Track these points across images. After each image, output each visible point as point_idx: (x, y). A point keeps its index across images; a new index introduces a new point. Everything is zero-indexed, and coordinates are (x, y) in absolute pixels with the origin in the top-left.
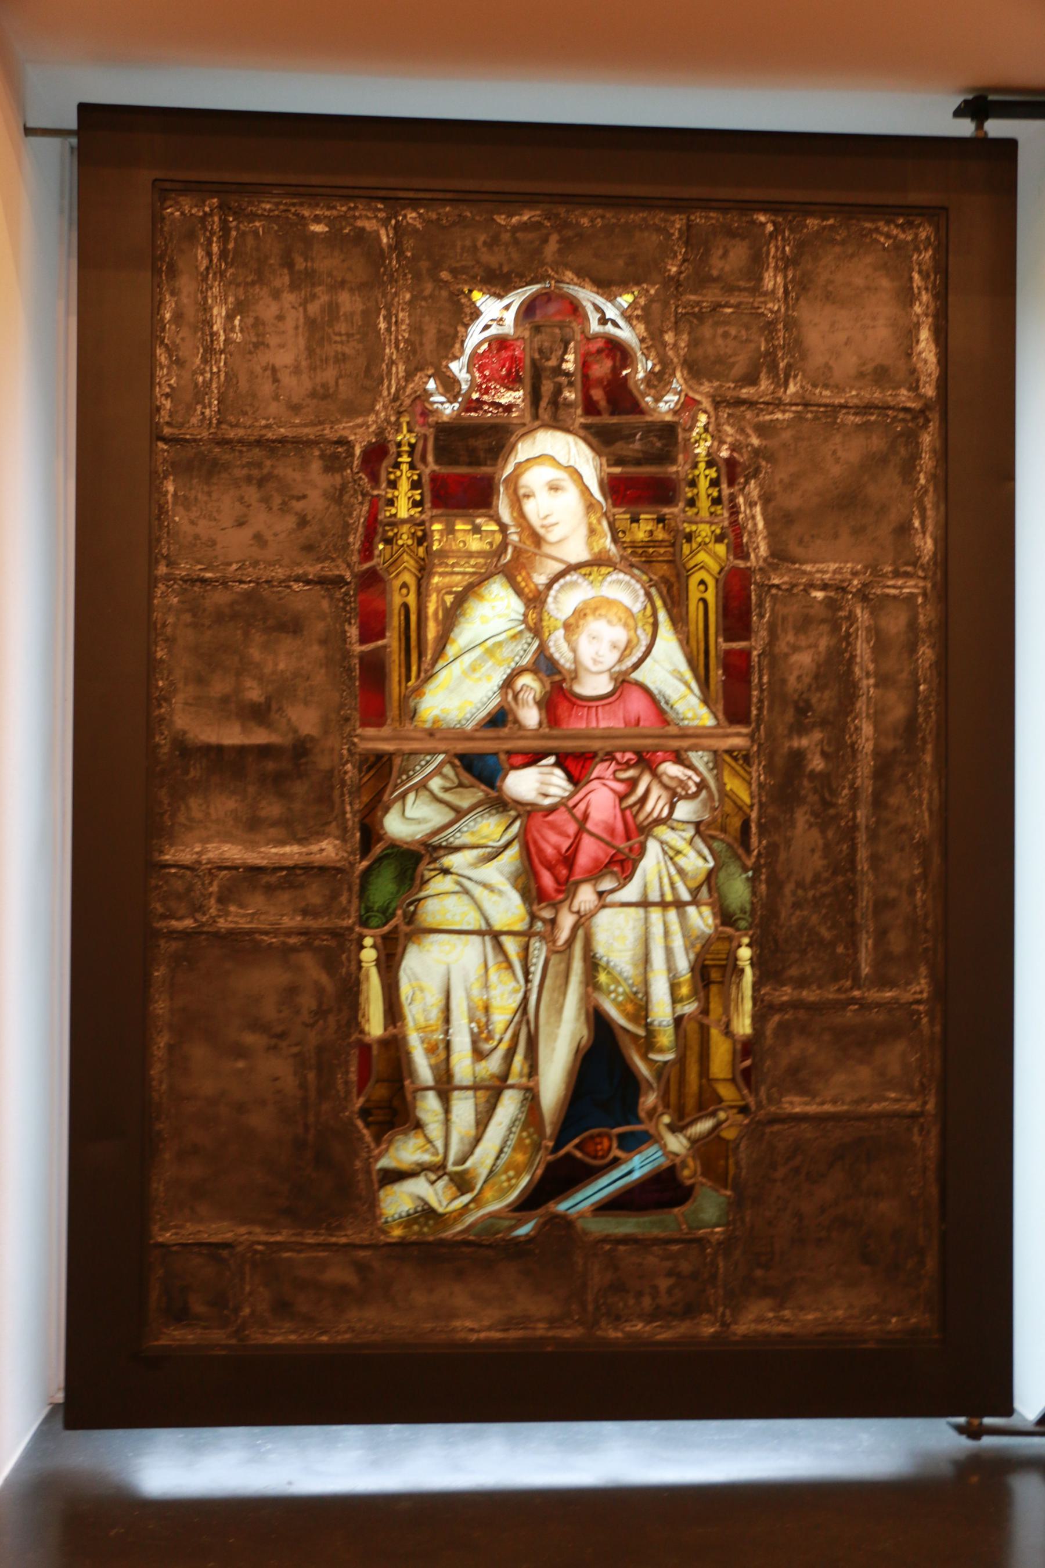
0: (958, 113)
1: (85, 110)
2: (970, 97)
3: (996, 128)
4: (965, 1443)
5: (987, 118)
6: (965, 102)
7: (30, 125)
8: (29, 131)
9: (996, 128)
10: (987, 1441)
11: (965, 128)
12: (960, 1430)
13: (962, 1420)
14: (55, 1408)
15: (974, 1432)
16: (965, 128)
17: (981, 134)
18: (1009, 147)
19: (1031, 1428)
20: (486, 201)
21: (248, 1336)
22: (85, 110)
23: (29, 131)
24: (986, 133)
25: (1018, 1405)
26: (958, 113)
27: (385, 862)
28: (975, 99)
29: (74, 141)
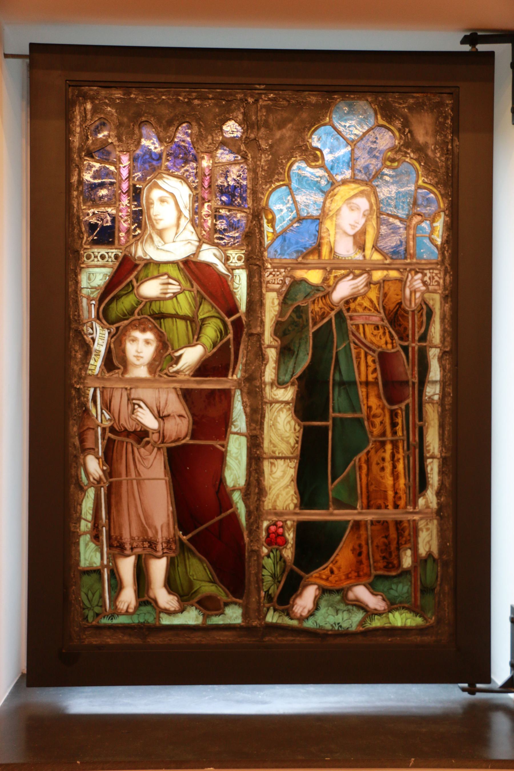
0: (463, 42)
1: (32, 46)
2: (468, 34)
3: (481, 47)
4: (466, 695)
5: (477, 43)
6: (466, 37)
7: (6, 53)
8: (6, 56)
9: (481, 47)
10: (479, 696)
11: (467, 48)
12: (464, 690)
13: (466, 685)
14: (23, 675)
15: (472, 691)
16: (467, 48)
17: (474, 50)
18: (491, 55)
19: (499, 689)
20: (142, 504)
21: (164, 177)
22: (32, 46)
23: (6, 56)
24: (477, 49)
25: (493, 677)
26: (463, 42)
27: (173, 438)
28: (471, 34)
29: (28, 60)
